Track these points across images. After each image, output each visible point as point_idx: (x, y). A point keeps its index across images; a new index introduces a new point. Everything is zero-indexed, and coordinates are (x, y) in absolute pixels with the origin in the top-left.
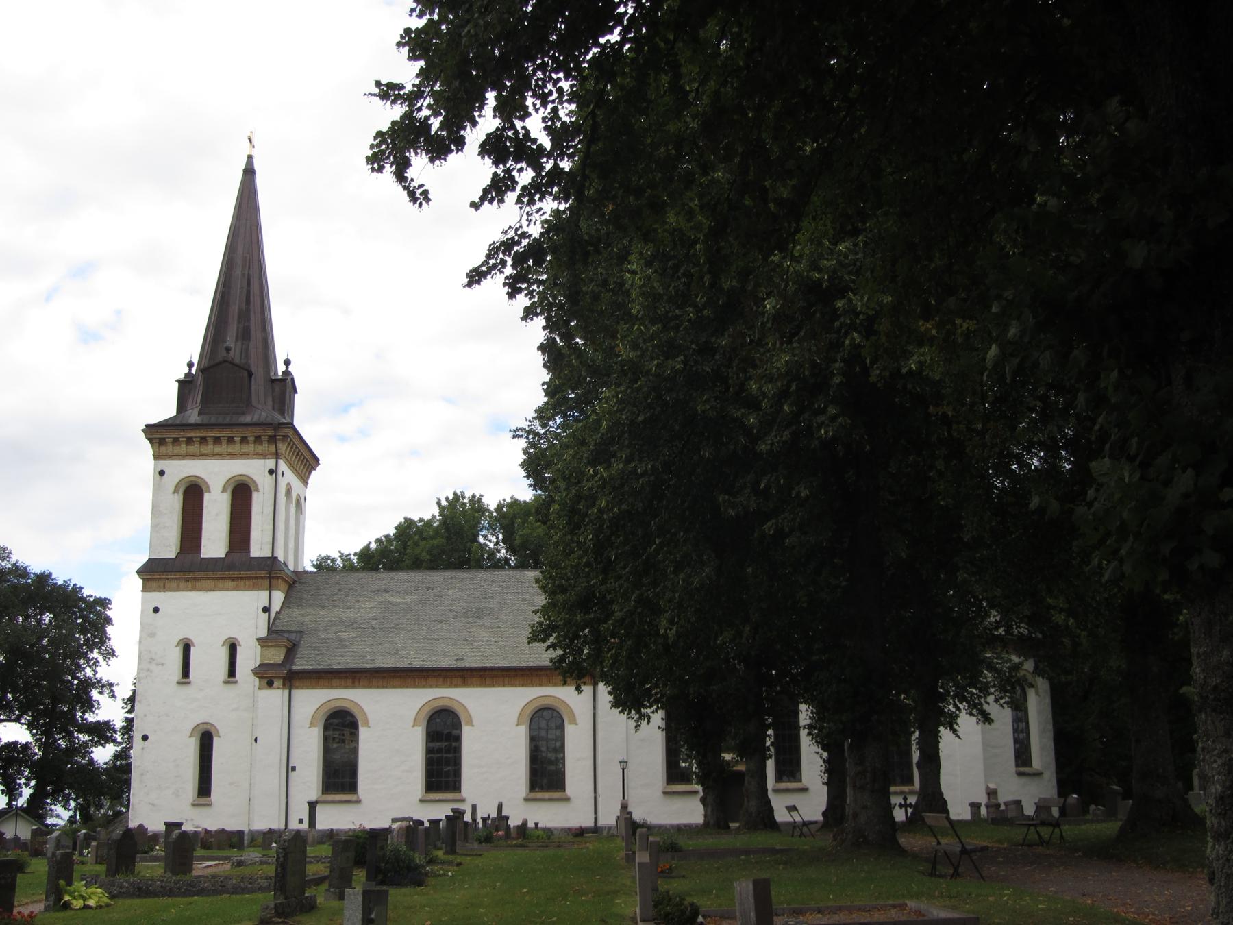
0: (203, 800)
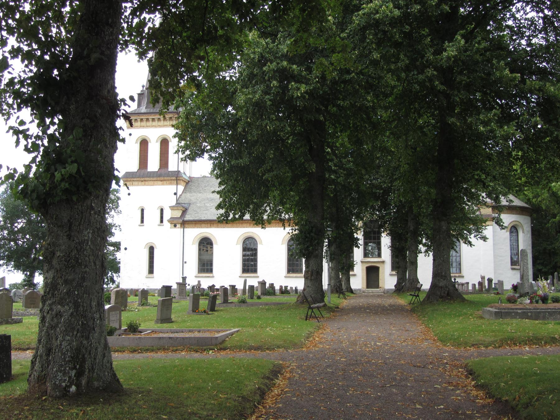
0: (151, 275)
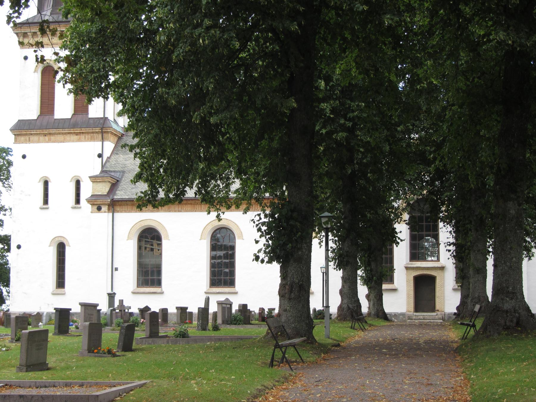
0: (60, 291)
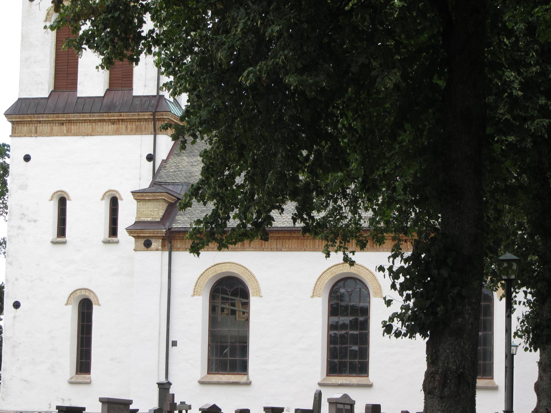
0: (82, 377)
